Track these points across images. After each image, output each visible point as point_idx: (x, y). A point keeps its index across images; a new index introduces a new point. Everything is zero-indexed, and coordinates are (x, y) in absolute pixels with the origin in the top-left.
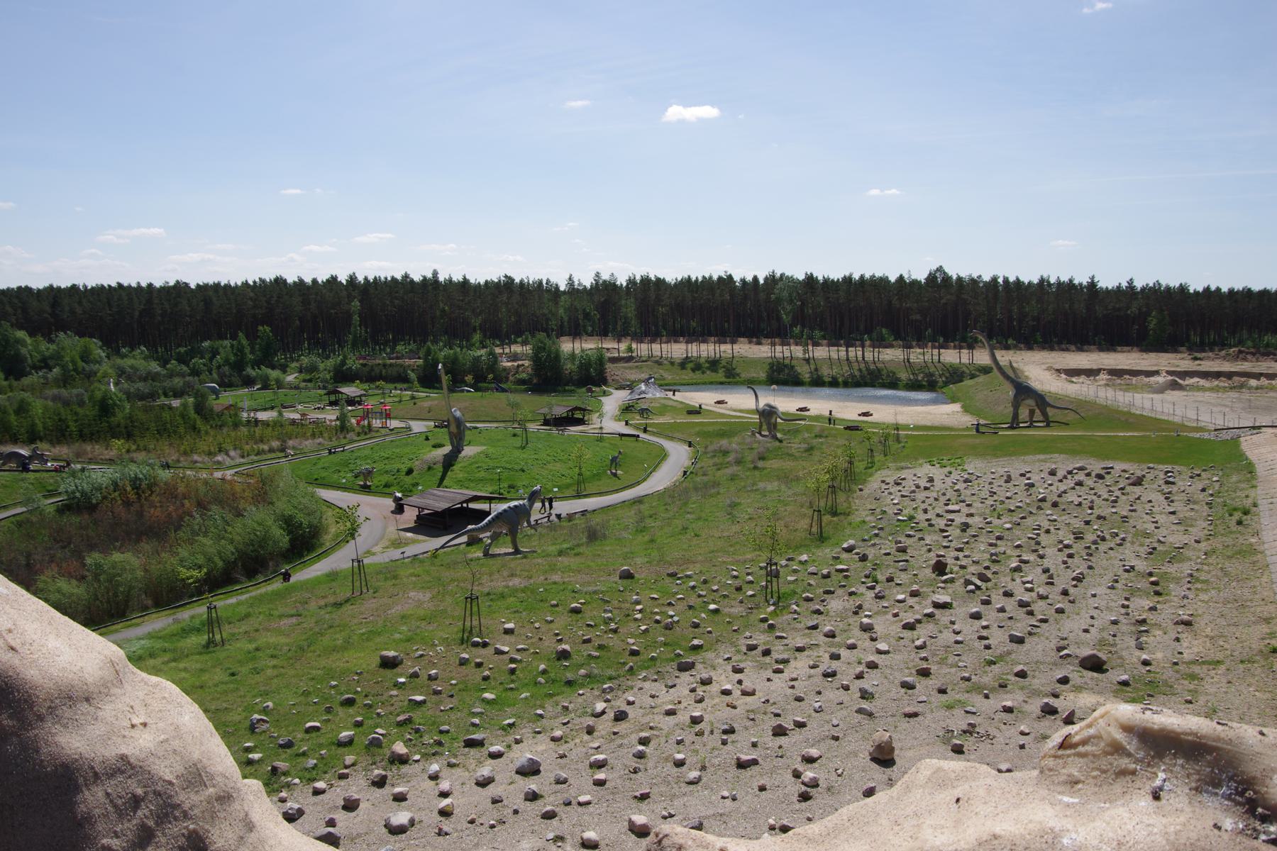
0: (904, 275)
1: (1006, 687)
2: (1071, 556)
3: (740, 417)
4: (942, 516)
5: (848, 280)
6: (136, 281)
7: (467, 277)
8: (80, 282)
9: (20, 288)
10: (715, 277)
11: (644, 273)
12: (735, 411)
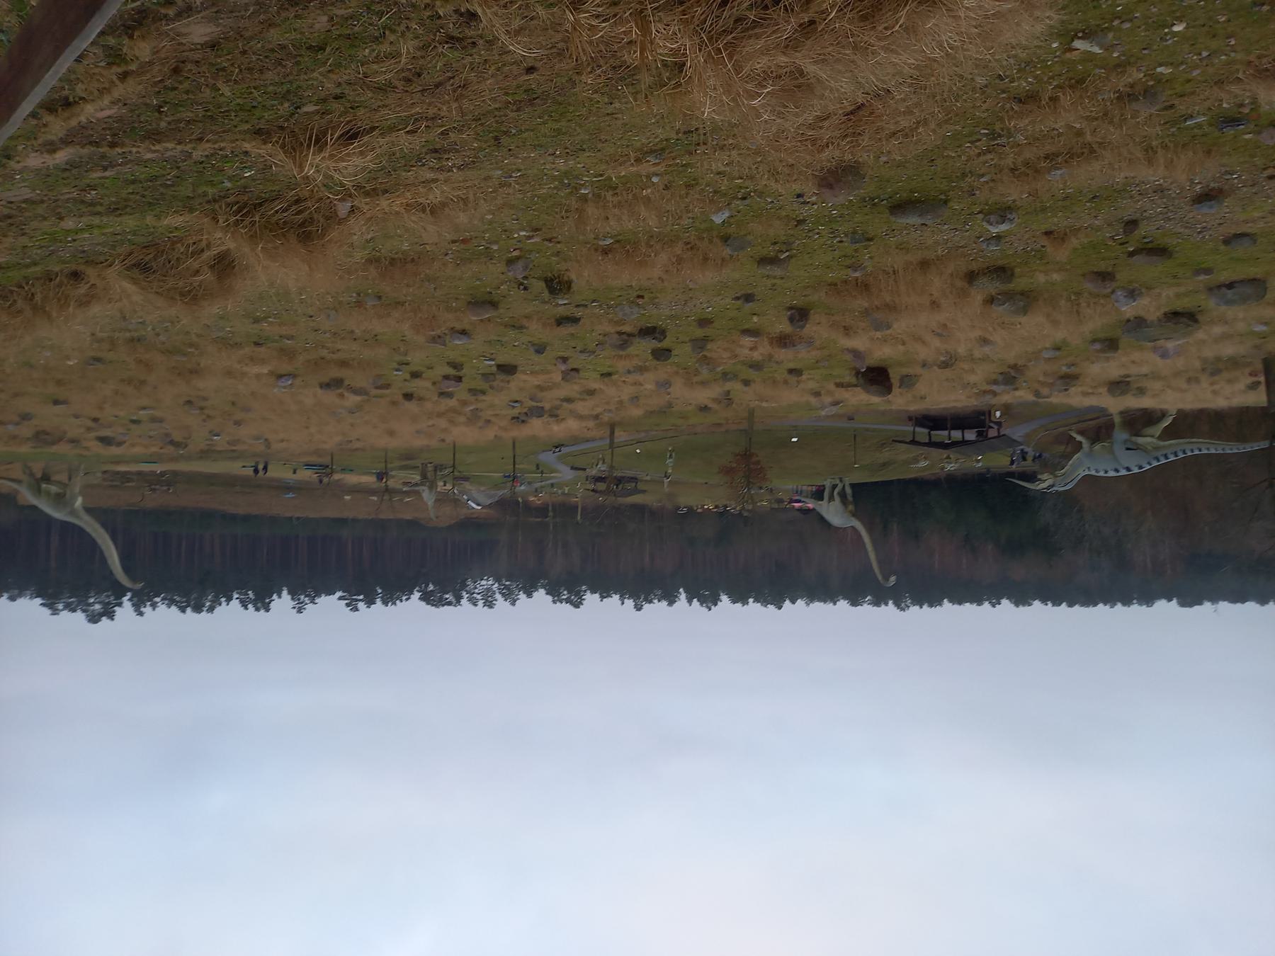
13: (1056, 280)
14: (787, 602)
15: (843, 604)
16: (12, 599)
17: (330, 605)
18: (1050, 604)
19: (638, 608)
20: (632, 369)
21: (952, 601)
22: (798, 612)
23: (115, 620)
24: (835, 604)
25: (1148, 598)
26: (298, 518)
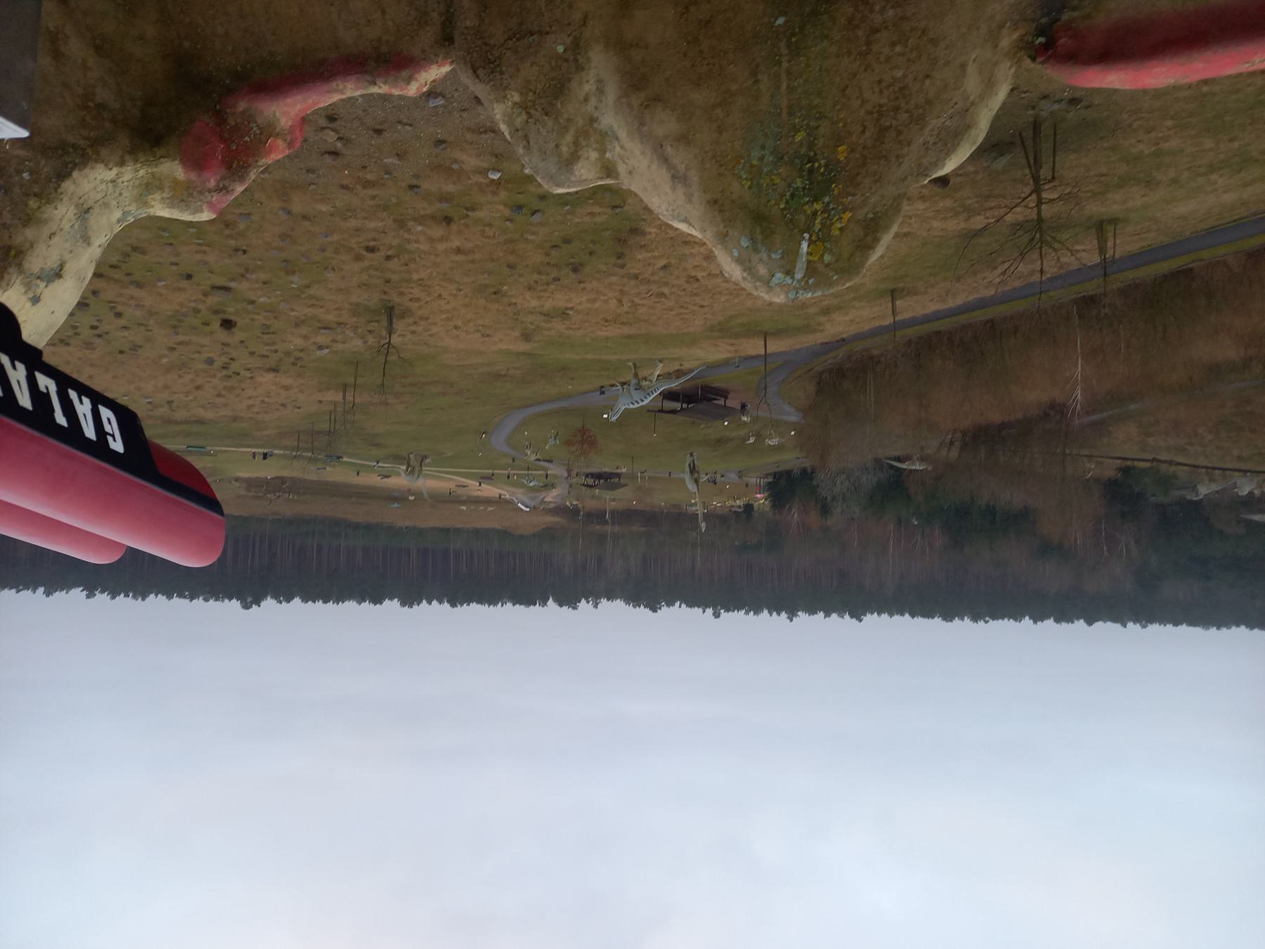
0: (427, 605)
1: (559, 279)
2: (93, 328)
3: (454, 473)
4: (234, 373)
5: (1176, 624)
6: (846, 620)
7: (769, 615)
8: (184, 602)
9: (377, 600)
10: (297, 601)
11: (1135, 626)
12: (442, 477)
13: (56, 208)
14: (766, 612)
15: (1081, 624)
16: (48, 593)
17: (1050, 622)
18: (847, 616)
19: (717, 615)
20: (240, 252)
21: (276, 597)
22: (874, 622)
23: (48, 598)
24: (113, 598)
25: (339, 599)
26: (407, 528)
